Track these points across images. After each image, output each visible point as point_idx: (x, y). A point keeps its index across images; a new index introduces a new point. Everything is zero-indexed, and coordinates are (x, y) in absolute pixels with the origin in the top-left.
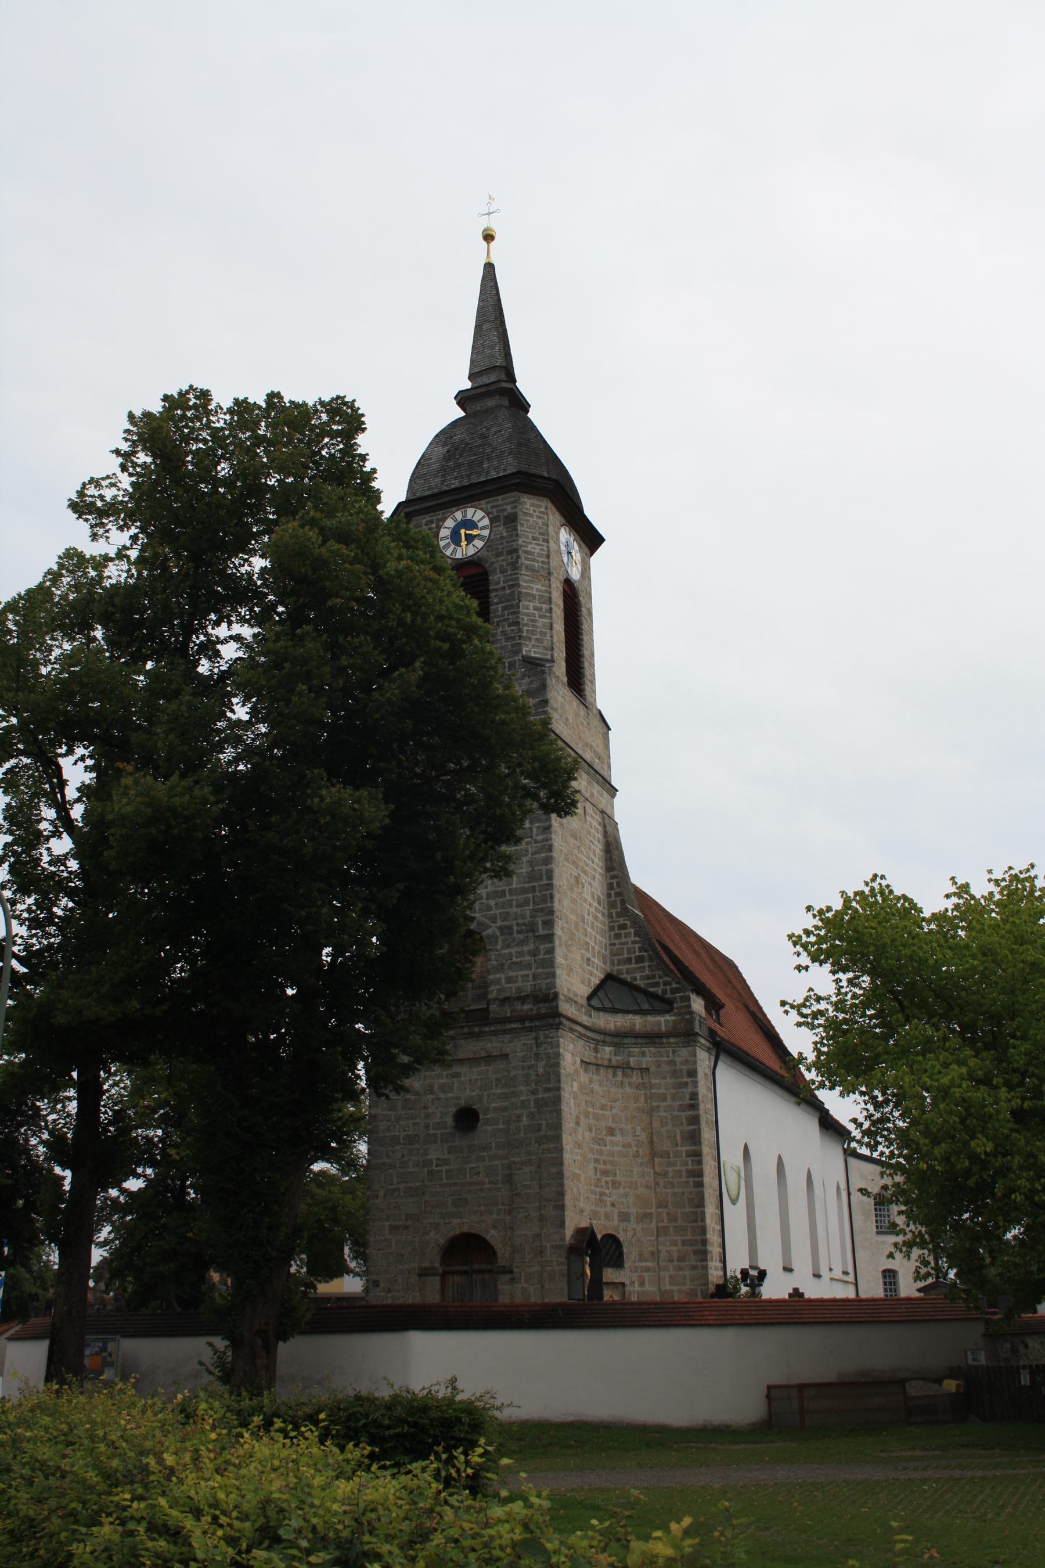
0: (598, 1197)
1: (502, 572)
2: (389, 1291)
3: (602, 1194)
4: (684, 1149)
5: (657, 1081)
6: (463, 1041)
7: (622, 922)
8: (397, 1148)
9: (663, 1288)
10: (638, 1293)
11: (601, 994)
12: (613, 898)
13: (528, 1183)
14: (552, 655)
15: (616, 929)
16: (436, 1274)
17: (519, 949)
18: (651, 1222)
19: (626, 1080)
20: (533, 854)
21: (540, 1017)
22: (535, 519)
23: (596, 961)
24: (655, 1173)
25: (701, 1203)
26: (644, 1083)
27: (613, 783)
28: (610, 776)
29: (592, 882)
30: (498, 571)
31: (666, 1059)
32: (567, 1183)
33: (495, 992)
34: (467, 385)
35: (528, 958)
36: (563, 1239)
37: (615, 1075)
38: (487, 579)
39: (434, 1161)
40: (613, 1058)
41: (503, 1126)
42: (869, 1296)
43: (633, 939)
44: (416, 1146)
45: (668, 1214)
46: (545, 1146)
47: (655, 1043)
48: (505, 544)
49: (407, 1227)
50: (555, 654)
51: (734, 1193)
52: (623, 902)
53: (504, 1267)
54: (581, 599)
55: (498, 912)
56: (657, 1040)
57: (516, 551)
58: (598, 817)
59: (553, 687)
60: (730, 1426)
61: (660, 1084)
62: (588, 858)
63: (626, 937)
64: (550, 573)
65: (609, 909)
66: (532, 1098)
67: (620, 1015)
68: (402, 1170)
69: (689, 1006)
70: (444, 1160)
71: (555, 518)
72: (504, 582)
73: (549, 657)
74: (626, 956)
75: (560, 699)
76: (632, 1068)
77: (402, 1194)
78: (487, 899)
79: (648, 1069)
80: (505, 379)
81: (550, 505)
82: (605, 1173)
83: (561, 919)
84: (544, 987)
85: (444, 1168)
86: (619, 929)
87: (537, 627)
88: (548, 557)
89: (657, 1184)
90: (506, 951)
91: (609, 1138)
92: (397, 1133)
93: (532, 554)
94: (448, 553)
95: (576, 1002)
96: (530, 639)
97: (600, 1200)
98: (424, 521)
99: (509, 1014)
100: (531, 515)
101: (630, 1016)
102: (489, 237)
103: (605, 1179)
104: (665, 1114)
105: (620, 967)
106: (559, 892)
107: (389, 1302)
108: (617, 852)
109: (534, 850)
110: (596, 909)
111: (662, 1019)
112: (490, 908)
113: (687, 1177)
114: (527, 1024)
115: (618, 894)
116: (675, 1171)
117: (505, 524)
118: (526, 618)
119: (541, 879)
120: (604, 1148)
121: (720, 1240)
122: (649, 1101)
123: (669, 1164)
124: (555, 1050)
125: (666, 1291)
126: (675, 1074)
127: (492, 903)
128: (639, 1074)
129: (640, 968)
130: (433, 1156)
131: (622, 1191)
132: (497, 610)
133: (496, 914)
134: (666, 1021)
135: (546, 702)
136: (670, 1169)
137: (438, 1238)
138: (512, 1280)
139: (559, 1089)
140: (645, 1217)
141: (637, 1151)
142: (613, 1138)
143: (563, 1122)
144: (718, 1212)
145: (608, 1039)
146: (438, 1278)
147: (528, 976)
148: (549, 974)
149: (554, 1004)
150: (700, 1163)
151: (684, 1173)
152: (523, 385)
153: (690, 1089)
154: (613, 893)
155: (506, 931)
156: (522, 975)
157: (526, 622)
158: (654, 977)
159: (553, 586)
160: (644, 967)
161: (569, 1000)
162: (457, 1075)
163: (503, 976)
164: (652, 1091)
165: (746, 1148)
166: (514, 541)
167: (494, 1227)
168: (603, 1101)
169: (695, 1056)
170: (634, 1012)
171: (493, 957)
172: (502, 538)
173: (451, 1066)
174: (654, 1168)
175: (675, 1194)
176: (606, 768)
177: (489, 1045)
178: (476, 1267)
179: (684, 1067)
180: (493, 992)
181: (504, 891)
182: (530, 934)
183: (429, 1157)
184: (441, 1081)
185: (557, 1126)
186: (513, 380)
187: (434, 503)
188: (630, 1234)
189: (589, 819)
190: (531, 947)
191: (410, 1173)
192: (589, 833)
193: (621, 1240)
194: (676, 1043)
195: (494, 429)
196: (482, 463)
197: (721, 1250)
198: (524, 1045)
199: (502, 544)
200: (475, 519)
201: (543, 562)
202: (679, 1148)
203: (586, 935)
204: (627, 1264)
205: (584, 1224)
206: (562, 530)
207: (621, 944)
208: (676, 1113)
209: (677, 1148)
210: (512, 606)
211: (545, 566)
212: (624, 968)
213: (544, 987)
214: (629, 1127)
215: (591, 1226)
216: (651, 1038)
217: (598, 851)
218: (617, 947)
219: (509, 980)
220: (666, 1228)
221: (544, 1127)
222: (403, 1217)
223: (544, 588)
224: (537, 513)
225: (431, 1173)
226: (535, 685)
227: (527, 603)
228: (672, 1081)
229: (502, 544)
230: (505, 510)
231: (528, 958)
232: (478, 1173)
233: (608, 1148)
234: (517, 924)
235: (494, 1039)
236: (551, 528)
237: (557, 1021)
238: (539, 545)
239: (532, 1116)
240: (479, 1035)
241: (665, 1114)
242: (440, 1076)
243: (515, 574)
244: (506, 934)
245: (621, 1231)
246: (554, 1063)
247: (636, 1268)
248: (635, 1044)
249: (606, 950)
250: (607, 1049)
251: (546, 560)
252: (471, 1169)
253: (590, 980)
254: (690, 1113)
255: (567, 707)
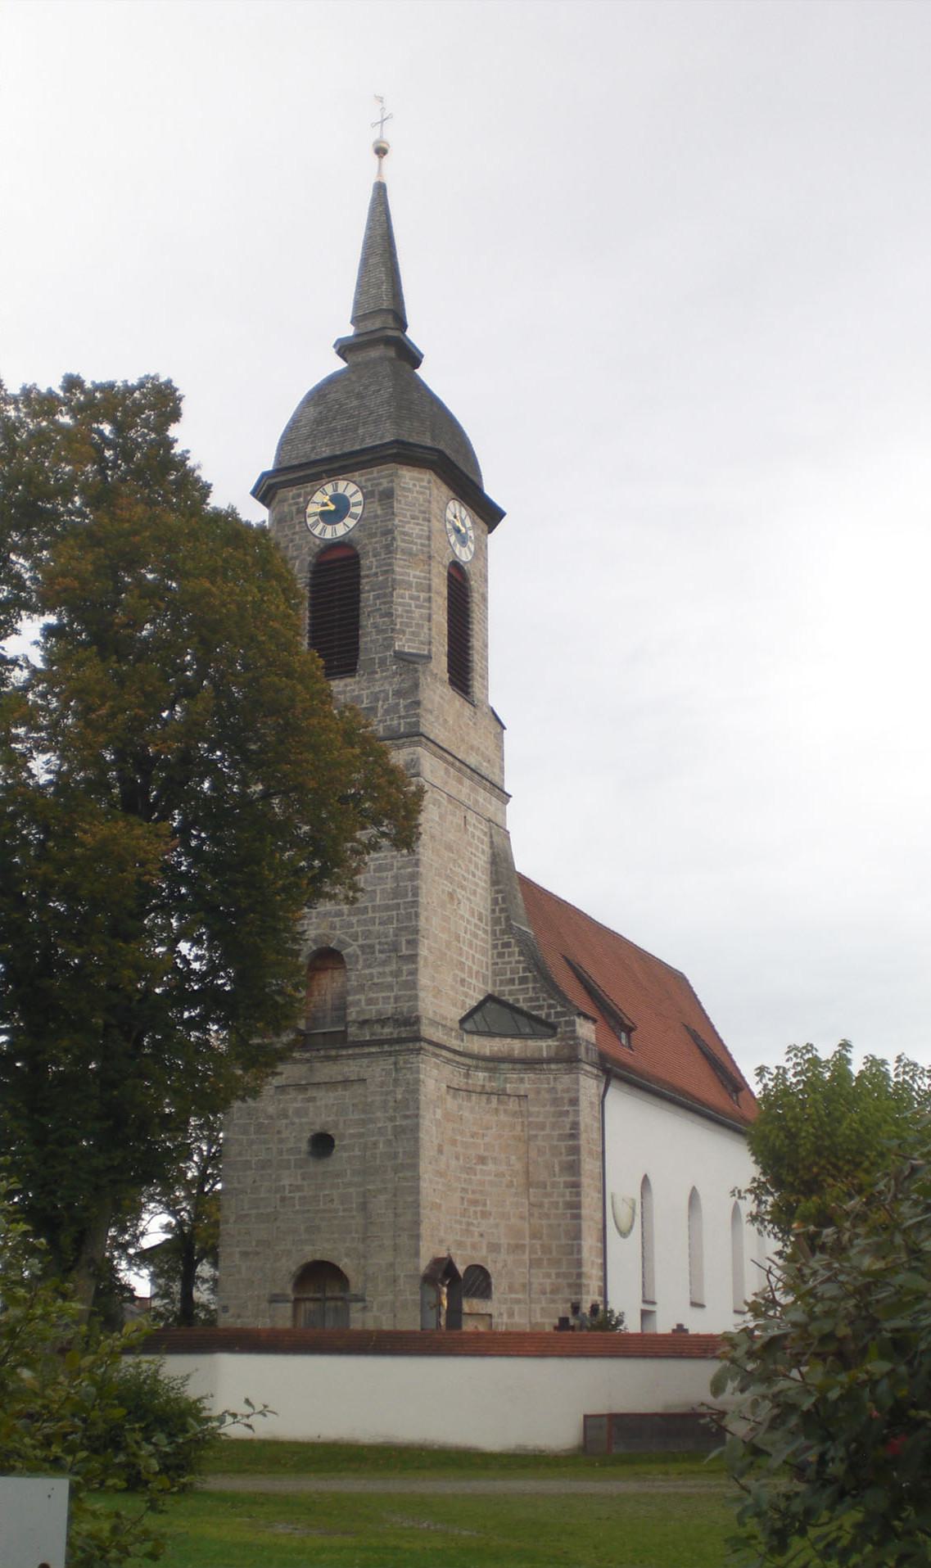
0: (464, 1227)
1: (375, 556)
2: (239, 1316)
3: (469, 1224)
4: (562, 1180)
5: (537, 1109)
6: (318, 1064)
7: (506, 940)
8: (249, 1173)
9: (534, 1321)
10: (507, 1324)
11: (477, 1017)
12: (497, 914)
13: (383, 1211)
14: (430, 650)
15: (500, 947)
16: (288, 1301)
17: (381, 970)
18: (524, 1252)
19: (501, 1107)
20: (399, 869)
21: (400, 1041)
22: (415, 495)
23: (474, 981)
24: (530, 1204)
25: (577, 1235)
26: (521, 1111)
27: (506, 790)
28: (503, 780)
29: (472, 898)
30: (371, 554)
31: (546, 1086)
32: (425, 1212)
33: (354, 1013)
34: (349, 331)
35: (389, 979)
36: (417, 1269)
37: (489, 1101)
38: (358, 563)
39: (287, 1187)
40: (487, 1084)
41: (359, 1153)
42: (695, 1333)
43: (517, 958)
44: (269, 1172)
45: (542, 1245)
46: (401, 1175)
47: (535, 1069)
48: (408, 514)
49: (257, 1253)
50: (434, 649)
51: (624, 1222)
52: (508, 919)
53: (356, 1295)
54: (472, 583)
55: (359, 929)
56: (537, 1066)
57: (391, 532)
58: (484, 827)
59: (428, 686)
60: (543, 1451)
61: (539, 1112)
62: (467, 871)
63: (509, 956)
64: (430, 557)
65: (492, 926)
66: (390, 1125)
67: (497, 1039)
68: (254, 1196)
69: (574, 1031)
70: (297, 1186)
71: (439, 491)
72: (377, 568)
73: (426, 652)
74: (508, 976)
75: (437, 699)
76: (509, 1095)
77: (253, 1220)
78: (348, 915)
79: (526, 1096)
80: (392, 326)
81: (433, 477)
82: (475, 1202)
83: (427, 938)
84: (405, 1010)
85: (298, 1195)
86: (502, 948)
87: (411, 618)
88: (429, 538)
89: (531, 1215)
90: (367, 971)
91: (479, 1167)
92: (249, 1158)
93: (410, 535)
94: (316, 532)
95: (444, 1026)
96: (404, 632)
97: (467, 1230)
98: (291, 494)
99: (368, 1038)
100: (409, 490)
101: (509, 1040)
102: (381, 152)
103: (472, 1209)
104: (543, 1144)
105: (502, 988)
106: (426, 910)
107: (239, 1326)
108: (505, 865)
109: (400, 864)
110: (476, 925)
111: (543, 1044)
112: (351, 925)
113: (564, 1209)
114: (386, 1048)
115: (502, 910)
116: (552, 1203)
117: (380, 501)
118: (400, 609)
119: (406, 895)
120: (473, 1177)
121: (601, 1274)
122: (526, 1129)
123: (547, 1195)
124: (416, 1076)
125: (537, 1323)
126: (556, 1102)
127: (354, 919)
128: (517, 1101)
129: (523, 989)
130: (286, 1182)
131: (492, 1221)
132: (368, 599)
133: (357, 932)
134: (549, 1047)
135: (418, 703)
136: (546, 1201)
137: (291, 1265)
138: (364, 1309)
139: (417, 1116)
140: (517, 1248)
141: (512, 1182)
142: (484, 1168)
143: (421, 1151)
144: (600, 1245)
145: (481, 1064)
146: (289, 1305)
147: (389, 998)
148: (410, 996)
149: (415, 1028)
150: (578, 1194)
151: (561, 1204)
152: (414, 334)
153: (571, 1118)
154: (497, 909)
155: (368, 950)
156: (383, 998)
157: (399, 613)
158: (537, 999)
159: (434, 571)
160: (528, 988)
161: (434, 1023)
162: (312, 1099)
163: (362, 997)
164: (530, 1119)
165: (646, 1180)
166: (389, 520)
167: (347, 1255)
168: (475, 1129)
169: (578, 1084)
170: (513, 1036)
171: (353, 978)
172: (376, 516)
173: (307, 1089)
174: (529, 1199)
175: (550, 1226)
176: (497, 771)
177: (346, 1069)
178: (329, 1294)
179: (565, 1095)
180: (353, 1014)
181: (366, 908)
182: (392, 954)
183: (282, 1183)
184: (295, 1105)
185: (415, 1154)
186: (403, 326)
187: (302, 474)
188: (499, 1265)
189: (471, 829)
190: (394, 967)
191: (262, 1199)
192: (470, 844)
193: (490, 1271)
194: (557, 1070)
195: (373, 388)
196: (356, 429)
197: (601, 1284)
198: (383, 1070)
199: (376, 523)
200: (348, 494)
201: (422, 545)
202: (557, 1179)
203: (461, 955)
204: (495, 1295)
205: (444, 1254)
206: (451, 504)
207: (503, 963)
208: (555, 1143)
209: (555, 1179)
210: (385, 595)
211: (425, 549)
212: (507, 989)
213: (405, 1010)
214: (503, 1156)
215: (449, 1255)
216: (530, 1063)
217: (481, 863)
218: (500, 966)
219: (370, 1001)
220: (540, 1260)
221: (401, 1155)
222: (254, 1243)
223: (423, 574)
224: (418, 488)
225: (283, 1199)
226: (405, 685)
227: (402, 591)
228: (552, 1109)
229: (376, 523)
230: (380, 484)
231: (389, 979)
232: (332, 1201)
233: (478, 1177)
234: (380, 943)
235: (351, 1062)
236: (434, 506)
237: (417, 1045)
238: (418, 524)
239: (389, 1143)
240: (336, 1058)
241: (543, 1144)
242: (295, 1099)
243: (389, 558)
244: (368, 954)
245: (489, 1262)
246: (414, 1089)
247: (506, 1299)
248: (514, 1070)
249: (487, 970)
250: (481, 1075)
251: (427, 542)
252: (325, 1196)
253: (464, 1003)
254: (571, 1143)
255: (446, 706)
